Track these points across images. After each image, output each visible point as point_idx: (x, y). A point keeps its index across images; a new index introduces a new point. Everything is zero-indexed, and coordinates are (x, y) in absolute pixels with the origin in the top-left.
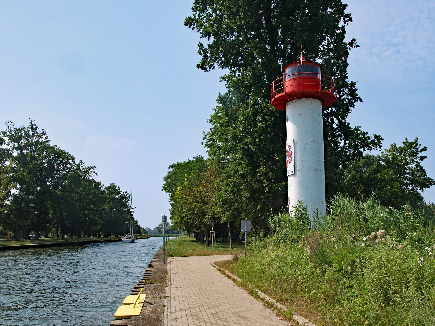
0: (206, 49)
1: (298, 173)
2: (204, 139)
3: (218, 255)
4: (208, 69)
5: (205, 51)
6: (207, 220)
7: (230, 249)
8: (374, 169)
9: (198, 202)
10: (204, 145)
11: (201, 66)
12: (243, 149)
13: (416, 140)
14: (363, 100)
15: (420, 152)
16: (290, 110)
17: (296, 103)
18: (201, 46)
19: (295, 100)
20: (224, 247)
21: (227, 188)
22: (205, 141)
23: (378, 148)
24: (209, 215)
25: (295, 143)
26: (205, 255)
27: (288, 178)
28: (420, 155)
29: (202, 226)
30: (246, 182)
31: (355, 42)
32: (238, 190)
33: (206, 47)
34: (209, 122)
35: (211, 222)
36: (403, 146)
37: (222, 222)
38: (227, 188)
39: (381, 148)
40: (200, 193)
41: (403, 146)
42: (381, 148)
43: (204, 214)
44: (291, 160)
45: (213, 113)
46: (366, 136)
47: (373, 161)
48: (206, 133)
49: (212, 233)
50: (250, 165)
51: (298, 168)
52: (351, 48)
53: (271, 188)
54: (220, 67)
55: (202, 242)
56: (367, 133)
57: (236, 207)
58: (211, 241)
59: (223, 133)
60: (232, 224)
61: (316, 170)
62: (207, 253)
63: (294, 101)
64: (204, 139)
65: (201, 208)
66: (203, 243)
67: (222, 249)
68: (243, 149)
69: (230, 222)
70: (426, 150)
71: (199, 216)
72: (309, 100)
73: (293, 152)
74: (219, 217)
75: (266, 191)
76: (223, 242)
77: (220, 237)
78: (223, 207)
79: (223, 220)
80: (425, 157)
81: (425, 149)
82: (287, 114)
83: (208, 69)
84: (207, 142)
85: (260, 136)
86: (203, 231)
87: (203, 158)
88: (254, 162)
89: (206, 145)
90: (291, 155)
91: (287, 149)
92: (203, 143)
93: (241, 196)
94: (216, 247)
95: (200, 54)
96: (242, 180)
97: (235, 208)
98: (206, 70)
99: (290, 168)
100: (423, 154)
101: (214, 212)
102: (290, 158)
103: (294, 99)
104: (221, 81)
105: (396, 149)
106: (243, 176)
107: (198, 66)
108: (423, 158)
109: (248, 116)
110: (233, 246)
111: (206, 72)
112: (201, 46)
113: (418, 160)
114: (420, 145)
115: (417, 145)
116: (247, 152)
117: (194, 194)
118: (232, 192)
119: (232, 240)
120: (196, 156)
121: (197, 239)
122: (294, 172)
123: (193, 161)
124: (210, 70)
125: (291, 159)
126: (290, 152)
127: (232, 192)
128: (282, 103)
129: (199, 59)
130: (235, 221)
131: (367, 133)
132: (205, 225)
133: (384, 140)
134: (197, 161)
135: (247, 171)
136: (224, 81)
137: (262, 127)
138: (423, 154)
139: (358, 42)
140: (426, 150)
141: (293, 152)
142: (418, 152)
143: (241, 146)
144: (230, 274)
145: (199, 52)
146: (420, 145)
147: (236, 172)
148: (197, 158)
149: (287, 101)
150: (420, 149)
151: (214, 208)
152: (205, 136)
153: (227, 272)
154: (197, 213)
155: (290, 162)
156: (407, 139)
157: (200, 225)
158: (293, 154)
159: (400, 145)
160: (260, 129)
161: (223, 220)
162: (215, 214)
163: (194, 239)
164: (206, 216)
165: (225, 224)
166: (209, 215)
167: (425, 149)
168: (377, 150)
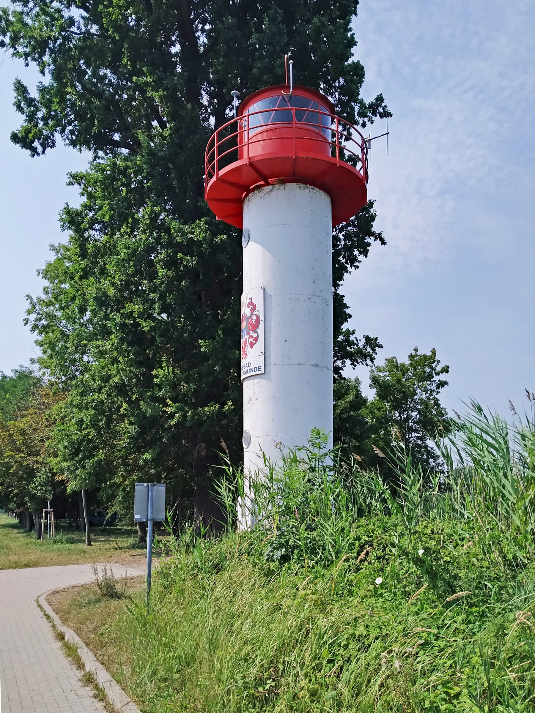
0: (33, 100)
1: (273, 370)
2: (29, 312)
3: (59, 564)
4: (40, 149)
5: (30, 102)
6: (36, 487)
7: (85, 546)
8: (350, 402)
9: (19, 450)
10: (29, 327)
11: (23, 139)
12: (123, 326)
13: (434, 353)
14: (386, 240)
15: (438, 374)
16: (259, 214)
17: (274, 194)
18: (21, 88)
19: (270, 187)
20: (71, 541)
21: (82, 415)
22: (33, 317)
23: (368, 361)
24: (42, 476)
25: (268, 297)
26: (27, 566)
27: (246, 384)
28: (436, 378)
29: (26, 499)
30: (129, 402)
31: (383, 105)
32: (109, 421)
33: (34, 94)
34: (41, 275)
35: (46, 491)
36: (407, 362)
37: (68, 491)
38: (82, 415)
39: (373, 362)
40: (23, 433)
41: (407, 362)
42: (373, 362)
43: (31, 473)
44: (256, 339)
45: (52, 257)
46: (352, 338)
47: (349, 389)
48: (35, 300)
49: (47, 513)
50: (139, 364)
51: (273, 359)
52: (374, 118)
53: (185, 416)
54: (67, 141)
55: (28, 528)
56: (353, 333)
57: (102, 457)
58: (46, 526)
59: (74, 297)
60: (92, 495)
61: (317, 366)
62: (32, 557)
63: (268, 188)
64: (29, 312)
65: (25, 463)
66: (30, 530)
67: (69, 546)
68: (123, 326)
69: (86, 491)
70: (447, 372)
71: (21, 479)
72: (307, 190)
73: (262, 318)
74: (63, 481)
75: (173, 423)
76: (69, 529)
77: (64, 517)
78: (72, 459)
79: (70, 487)
80: (446, 383)
81: (446, 370)
82: (247, 224)
83: (40, 149)
84: (36, 320)
85: (162, 297)
86: (28, 508)
87: (31, 372)
88: (148, 358)
89: (35, 327)
90: (255, 328)
91: (245, 311)
92: (26, 321)
93: (117, 434)
94: (55, 542)
95: (20, 109)
96: (120, 399)
97: (101, 460)
98: (35, 152)
99: (251, 358)
100: (443, 377)
101: (51, 470)
102: (252, 333)
103: (267, 184)
104: (71, 184)
105: (397, 367)
106: (122, 389)
107: (15, 138)
108: (442, 384)
109: (136, 250)
110: (92, 537)
111: (33, 156)
112: (21, 88)
113: (434, 387)
114: (439, 362)
115: (434, 361)
116: (133, 336)
117: (11, 435)
118: (95, 424)
119: (91, 524)
120: (18, 368)
121: (21, 522)
122: (262, 368)
123: (12, 379)
124: (43, 153)
125: (255, 336)
126: (254, 318)
127: (95, 424)
128: (237, 192)
129: (18, 122)
130: (99, 489)
131: (353, 333)
132: (33, 497)
133: (382, 347)
134: (20, 378)
135: (131, 378)
136: (76, 186)
137: (167, 276)
138: (443, 377)
139: (389, 104)
140: (447, 372)
141: (262, 318)
142: (434, 375)
143: (118, 320)
144: (103, 677)
145: (15, 104)
146: (439, 362)
147: (106, 379)
148: (19, 373)
149: (249, 191)
150: (439, 369)
151: (53, 461)
152: (34, 306)
153: (91, 663)
154: (15, 473)
155: (252, 345)
156: (416, 350)
157: (23, 497)
158: (262, 324)
159: (404, 360)
160: (163, 283)
161: (70, 487)
162: (54, 475)
163: (15, 521)
164: (35, 479)
165: (76, 494)
166: (42, 476)
167: (446, 370)
168: (367, 365)
